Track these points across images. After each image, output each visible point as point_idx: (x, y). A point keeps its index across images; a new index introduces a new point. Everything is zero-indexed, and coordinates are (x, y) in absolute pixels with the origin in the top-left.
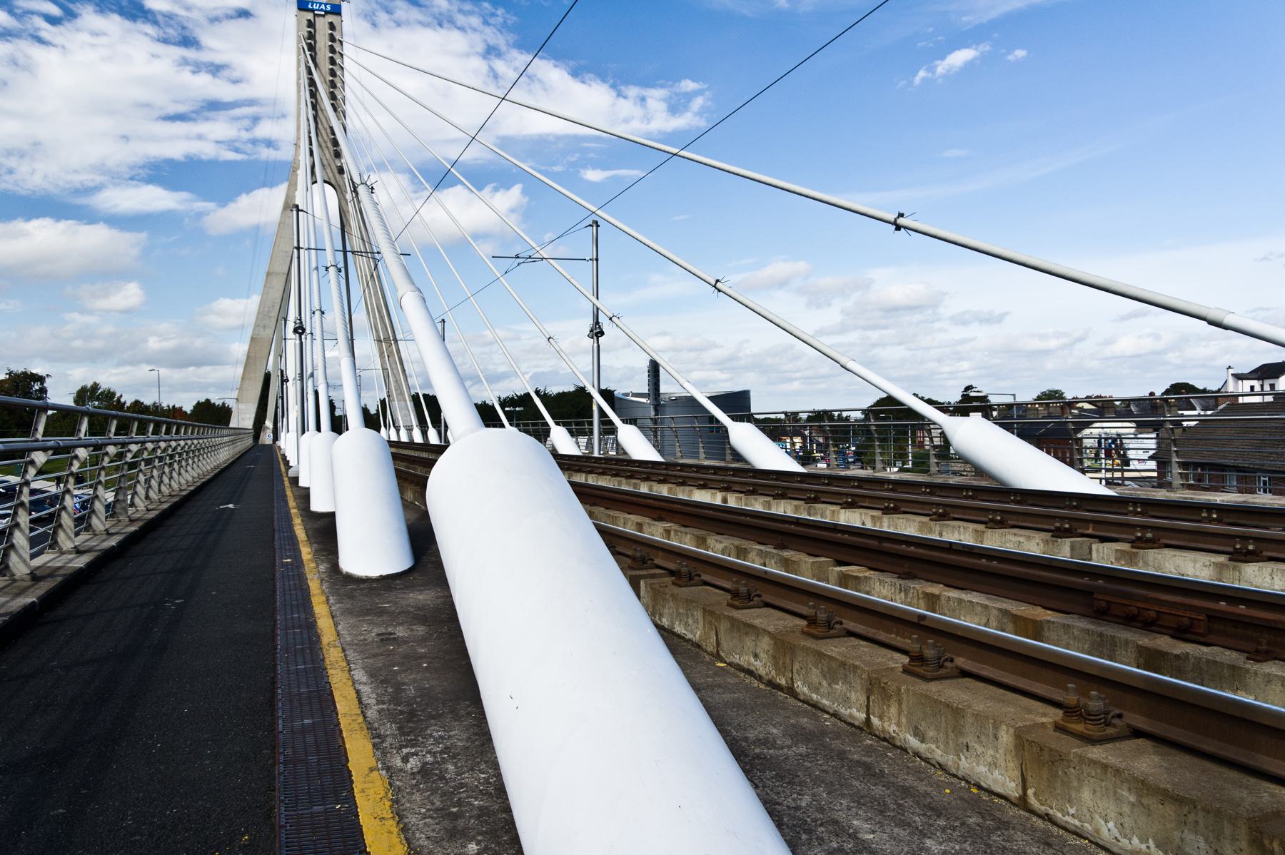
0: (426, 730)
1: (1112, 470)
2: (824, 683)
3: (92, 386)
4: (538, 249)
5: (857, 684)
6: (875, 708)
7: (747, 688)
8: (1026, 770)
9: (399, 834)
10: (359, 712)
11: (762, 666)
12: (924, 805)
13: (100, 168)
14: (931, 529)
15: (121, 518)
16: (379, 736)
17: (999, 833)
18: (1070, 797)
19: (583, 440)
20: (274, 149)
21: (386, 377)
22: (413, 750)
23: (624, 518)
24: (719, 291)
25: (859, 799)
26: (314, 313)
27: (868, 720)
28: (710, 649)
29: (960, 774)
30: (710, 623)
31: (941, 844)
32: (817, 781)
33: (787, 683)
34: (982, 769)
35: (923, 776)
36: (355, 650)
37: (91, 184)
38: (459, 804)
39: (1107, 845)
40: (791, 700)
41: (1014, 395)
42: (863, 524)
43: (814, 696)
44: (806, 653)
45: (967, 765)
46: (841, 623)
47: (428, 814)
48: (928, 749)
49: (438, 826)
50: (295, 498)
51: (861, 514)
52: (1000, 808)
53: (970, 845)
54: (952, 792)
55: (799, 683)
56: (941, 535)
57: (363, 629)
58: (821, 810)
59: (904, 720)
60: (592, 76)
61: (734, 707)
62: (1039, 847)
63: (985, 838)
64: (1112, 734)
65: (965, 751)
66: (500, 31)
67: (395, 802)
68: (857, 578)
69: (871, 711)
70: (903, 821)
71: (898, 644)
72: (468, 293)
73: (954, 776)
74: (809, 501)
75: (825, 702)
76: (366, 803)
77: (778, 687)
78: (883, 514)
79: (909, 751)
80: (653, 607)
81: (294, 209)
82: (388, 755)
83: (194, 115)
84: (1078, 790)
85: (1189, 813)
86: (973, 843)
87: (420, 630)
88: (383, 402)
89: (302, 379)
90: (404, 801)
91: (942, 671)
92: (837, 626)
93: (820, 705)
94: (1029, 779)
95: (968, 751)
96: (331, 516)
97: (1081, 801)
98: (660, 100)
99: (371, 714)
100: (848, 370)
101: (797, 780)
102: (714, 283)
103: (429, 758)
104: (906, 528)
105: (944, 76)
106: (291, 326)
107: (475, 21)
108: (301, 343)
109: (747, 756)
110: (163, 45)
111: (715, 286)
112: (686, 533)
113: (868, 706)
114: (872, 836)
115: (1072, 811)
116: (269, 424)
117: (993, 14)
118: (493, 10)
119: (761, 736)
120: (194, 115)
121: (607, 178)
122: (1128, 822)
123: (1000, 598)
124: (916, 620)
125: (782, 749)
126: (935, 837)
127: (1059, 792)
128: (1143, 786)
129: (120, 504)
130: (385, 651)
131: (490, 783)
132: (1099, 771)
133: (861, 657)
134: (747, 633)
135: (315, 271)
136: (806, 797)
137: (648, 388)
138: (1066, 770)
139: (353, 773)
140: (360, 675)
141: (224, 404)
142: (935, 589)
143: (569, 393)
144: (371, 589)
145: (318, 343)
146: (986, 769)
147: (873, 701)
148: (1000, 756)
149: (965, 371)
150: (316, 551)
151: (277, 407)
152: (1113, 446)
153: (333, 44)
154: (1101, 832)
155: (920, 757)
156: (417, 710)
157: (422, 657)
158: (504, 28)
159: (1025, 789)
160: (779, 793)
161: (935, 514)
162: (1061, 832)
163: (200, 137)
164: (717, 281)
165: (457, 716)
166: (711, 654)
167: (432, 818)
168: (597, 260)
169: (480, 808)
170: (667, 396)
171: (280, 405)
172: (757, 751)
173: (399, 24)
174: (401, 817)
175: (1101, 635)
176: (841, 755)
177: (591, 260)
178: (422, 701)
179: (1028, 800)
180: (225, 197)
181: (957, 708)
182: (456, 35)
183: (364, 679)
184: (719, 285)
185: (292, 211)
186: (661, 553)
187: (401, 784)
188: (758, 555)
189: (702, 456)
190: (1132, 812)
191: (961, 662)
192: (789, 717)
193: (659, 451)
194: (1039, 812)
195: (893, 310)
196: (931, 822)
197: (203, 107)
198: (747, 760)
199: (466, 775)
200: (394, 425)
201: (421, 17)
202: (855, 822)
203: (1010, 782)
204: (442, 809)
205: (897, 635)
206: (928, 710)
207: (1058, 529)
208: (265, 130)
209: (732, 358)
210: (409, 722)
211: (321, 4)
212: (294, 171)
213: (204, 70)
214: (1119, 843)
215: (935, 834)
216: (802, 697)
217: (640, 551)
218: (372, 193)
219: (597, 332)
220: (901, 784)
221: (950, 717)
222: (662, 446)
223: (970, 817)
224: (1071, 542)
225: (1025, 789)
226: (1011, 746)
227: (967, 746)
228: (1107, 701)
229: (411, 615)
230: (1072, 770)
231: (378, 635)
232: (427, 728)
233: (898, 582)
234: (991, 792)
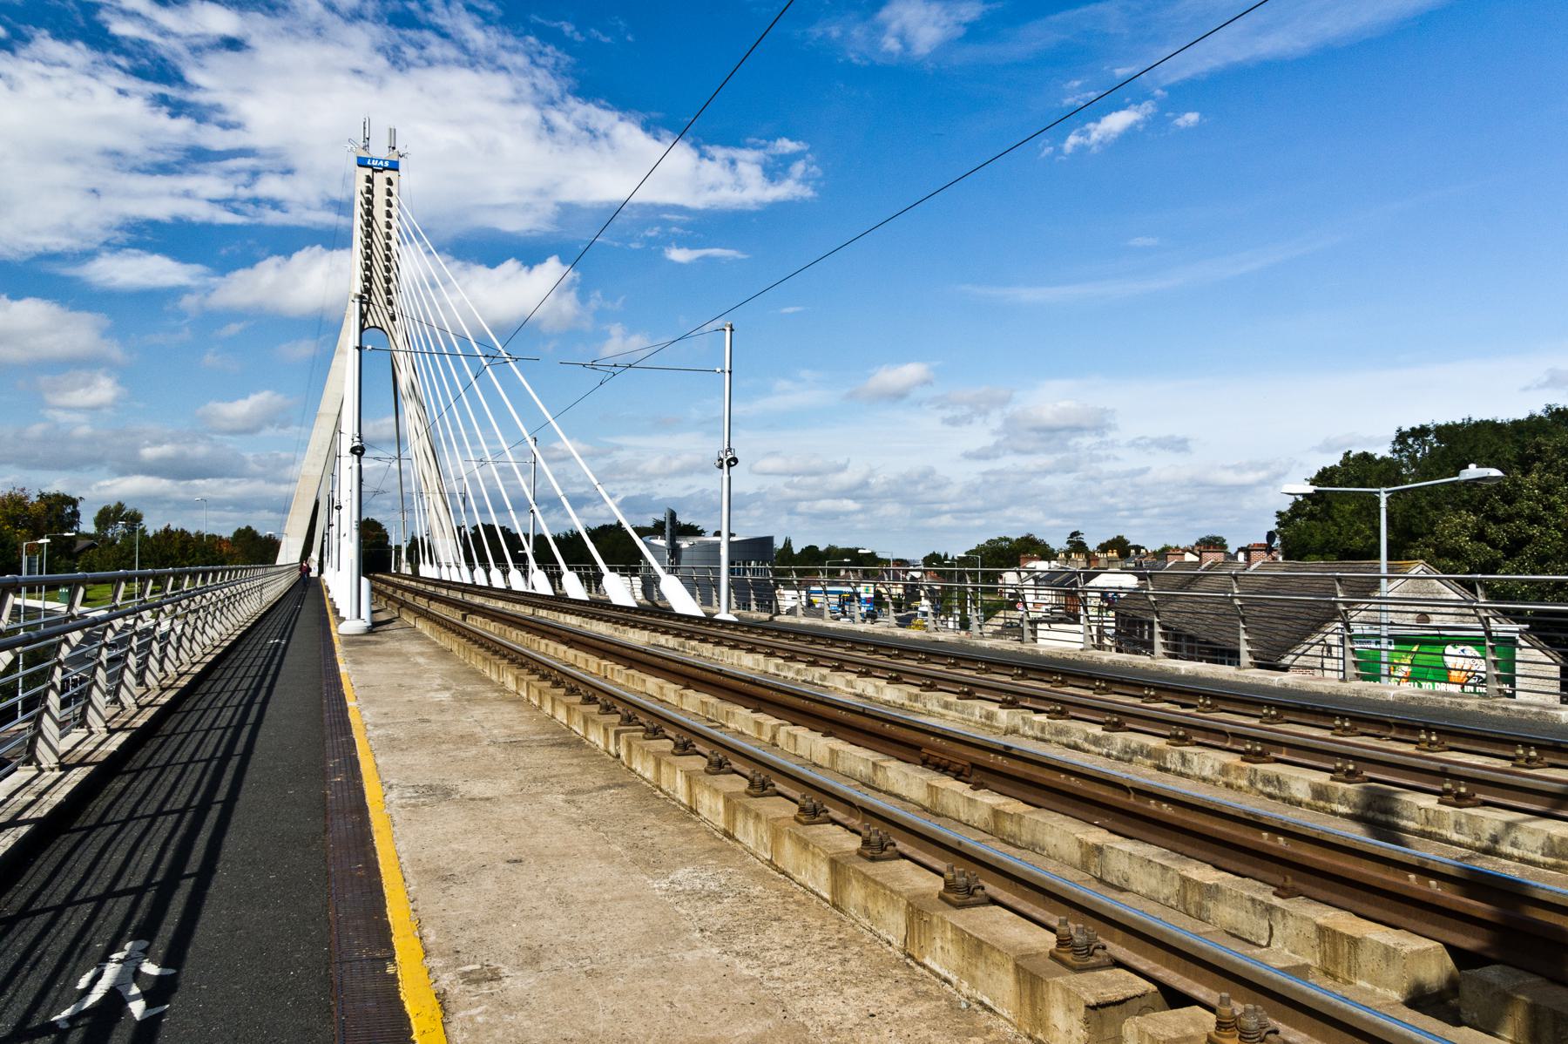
3: (115, 507)
20: (283, 211)
91: (1093, 960)
92: (979, 892)
98: (753, 163)
107: (520, 60)
118: (541, 48)
120: (178, 167)
121: (698, 259)
151: (323, 541)
158: (556, 71)
163: (187, 194)
173: (430, 63)
180: (225, 267)
209: (864, 484)
211: (379, 160)
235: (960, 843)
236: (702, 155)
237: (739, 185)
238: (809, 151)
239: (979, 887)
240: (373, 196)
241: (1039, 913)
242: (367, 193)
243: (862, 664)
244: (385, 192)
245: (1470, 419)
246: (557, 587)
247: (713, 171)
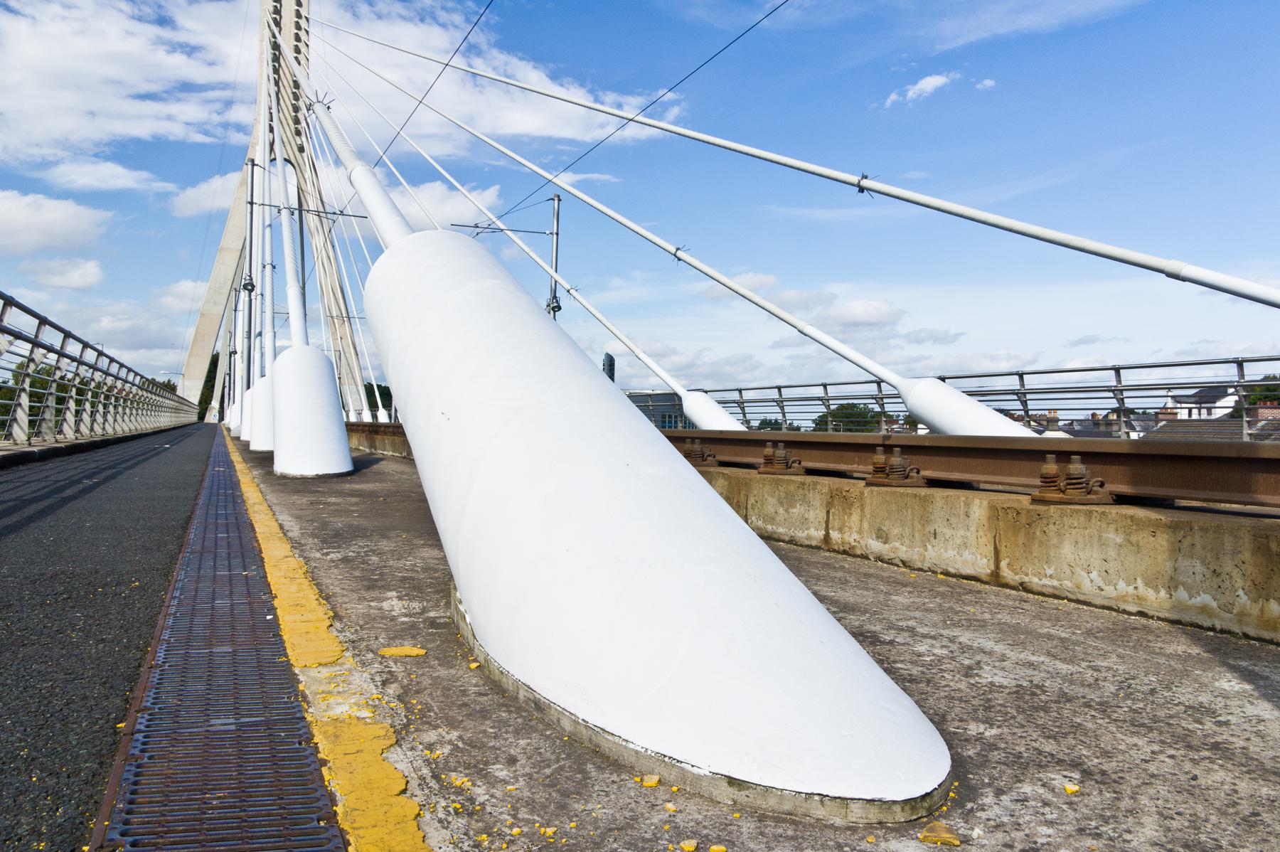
2: (781, 511)
6: (834, 522)
8: (1000, 541)
13: (64, 144)
15: (47, 438)
24: (679, 259)
26: (264, 267)
34: (951, 553)
37: (51, 159)
43: (769, 527)
44: (763, 484)
45: (935, 554)
59: (866, 525)
60: (571, 79)
65: (932, 539)
66: (482, 30)
69: (830, 526)
75: (781, 530)
79: (871, 557)
83: (165, 95)
85: (1185, 537)
89: (249, 337)
93: (776, 536)
94: (1003, 549)
95: (935, 538)
97: (1061, 558)
100: (805, 335)
105: (914, 101)
107: (458, 18)
110: (138, 22)
111: (675, 255)
113: (827, 523)
115: (1049, 572)
116: (215, 404)
117: (960, 42)
120: (165, 95)
122: (1113, 566)
127: (1036, 554)
129: (46, 423)
132: (1082, 519)
138: (1045, 529)
141: (169, 381)
148: (971, 535)
151: (224, 387)
153: (299, 21)
154: (1082, 587)
155: (882, 561)
163: (170, 118)
164: (678, 249)
168: (557, 234)
171: (227, 384)
173: (380, 17)
179: (1001, 573)
180: (192, 179)
182: (436, 31)
197: (174, 88)
201: (404, 12)
203: (981, 559)
205: (859, 465)
206: (893, 507)
208: (239, 114)
209: (691, 365)
213: (179, 50)
214: (1103, 593)
221: (917, 507)
226: (984, 521)
227: (935, 534)
230: (1051, 526)
240: (281, 17)
242: (274, 13)
244: (293, 14)
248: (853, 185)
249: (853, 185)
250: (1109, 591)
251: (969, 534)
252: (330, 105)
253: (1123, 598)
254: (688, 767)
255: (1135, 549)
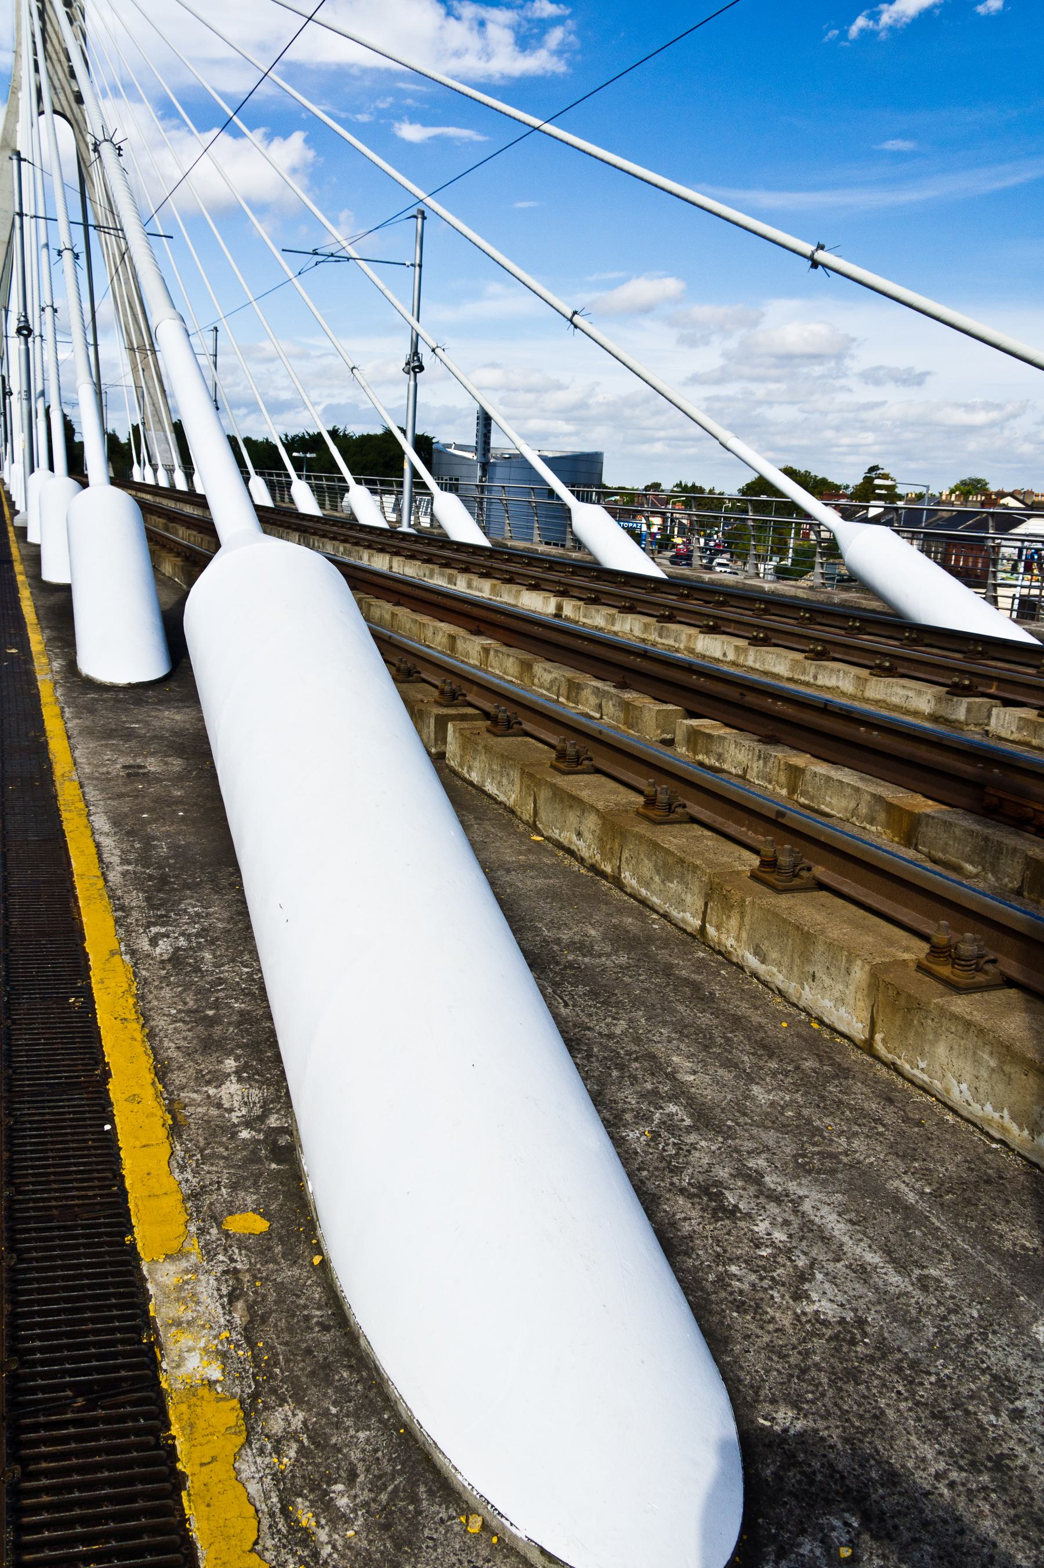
0: (180, 904)
1: (1030, 587)
2: (657, 879)
4: (345, 243)
5: (695, 887)
6: (713, 917)
7: (566, 872)
8: (877, 1012)
9: (143, 1042)
10: (99, 874)
11: (587, 848)
12: (756, 1042)
14: (805, 669)
16: (122, 908)
17: (836, 1082)
18: (923, 1050)
19: (389, 500)
21: (141, 398)
22: (163, 930)
23: (434, 627)
24: (576, 327)
25: (682, 1029)
26: (43, 310)
27: (703, 928)
28: (526, 817)
29: (801, 1004)
30: (528, 787)
31: (769, 1092)
32: (637, 1003)
33: (613, 871)
34: (827, 1003)
35: (759, 1003)
36: (96, 786)
38: (216, 1005)
39: (956, 1107)
40: (615, 892)
41: (928, 487)
42: (725, 655)
43: (643, 892)
45: (811, 996)
46: (684, 806)
47: (179, 1016)
48: (769, 971)
49: (190, 1034)
50: (23, 560)
51: (723, 643)
52: (841, 1050)
53: (802, 1095)
54: (789, 1026)
55: (627, 874)
56: (815, 677)
57: (106, 757)
58: (637, 1040)
59: (744, 935)
61: (547, 897)
62: (879, 1104)
63: (820, 1088)
64: (981, 982)
65: (810, 980)
67: (141, 997)
68: (710, 736)
69: (707, 919)
70: (729, 1060)
71: (749, 841)
72: (250, 295)
73: (794, 1005)
74: (663, 619)
76: (106, 998)
77: (603, 874)
78: (750, 644)
80: (462, 757)
81: (14, 157)
82: (133, 934)
84: (934, 1043)
86: (806, 1094)
87: (177, 764)
88: (136, 429)
90: (151, 996)
91: (796, 882)
92: (679, 810)
94: (879, 1023)
96: (67, 589)
99: (114, 877)
100: (728, 450)
101: (613, 999)
102: (569, 315)
103: (182, 942)
104: (774, 666)
105: (890, 29)
106: (13, 325)
108: (27, 350)
109: (557, 963)
111: (571, 321)
112: (508, 655)
113: (705, 913)
114: (692, 1077)
115: (922, 1065)
119: (577, 938)
121: (430, 138)
122: (983, 1087)
123: (875, 779)
124: (773, 816)
125: (600, 956)
126: (763, 1083)
128: (1006, 1052)
130: (132, 791)
131: (254, 980)
132: (960, 1028)
133: (703, 854)
134: (571, 807)
135: (45, 250)
136: (622, 1022)
137: (475, 439)
139: (91, 957)
140: (101, 822)
142: (800, 760)
143: (376, 436)
144: (117, 701)
145: (49, 345)
146: (832, 1004)
147: (712, 908)
149: (868, 445)
150: (49, 640)
152: (1036, 557)
155: (758, 979)
156: (169, 876)
157: (177, 802)
159: (872, 1032)
160: (591, 1015)
161: (811, 651)
162: (907, 1085)
164: (575, 313)
165: (217, 886)
166: (527, 823)
167: (184, 1022)
168: (420, 266)
169: (241, 1013)
170: (499, 452)
172: (571, 957)
174: (147, 1019)
175: (986, 839)
176: (668, 970)
177: (412, 265)
178: (176, 863)
181: (808, 933)
183: (106, 828)
184: (577, 319)
185: (11, 158)
186: (475, 688)
187: (148, 974)
188: (593, 693)
189: (537, 539)
190: (990, 1078)
191: (820, 871)
192: (611, 915)
193: (483, 528)
194: (885, 1060)
195: (787, 359)
196: (761, 1063)
198: (557, 969)
199: (226, 968)
200: (150, 461)
202: (674, 1059)
204: (196, 1011)
205: (749, 830)
206: (774, 929)
207: (955, 685)
209: (583, 405)
210: (159, 891)
212: (13, 93)
215: (764, 1080)
216: (629, 890)
217: (451, 684)
218: (120, 155)
219: (415, 366)
220: (732, 1012)
222: (489, 522)
223: (806, 1059)
224: (969, 703)
225: (872, 1032)
226: (864, 985)
227: (814, 976)
228: (982, 943)
229: (166, 743)
230: (929, 1021)
231: (125, 767)
232: (180, 901)
233: (759, 747)
234: (833, 1029)
235: (600, 732)
236: (450, 13)
237: (487, 54)
238: (570, 16)
239: (680, 805)
241: (731, 828)
243: (666, 606)
245: (286, 436)
246: (278, 499)
247: (459, 33)
248: (804, 256)
249: (804, 256)
250: (976, 1107)
251: (847, 992)
252: (122, 145)
253: (989, 1121)
254: (507, 1524)
255: (1006, 1079)
